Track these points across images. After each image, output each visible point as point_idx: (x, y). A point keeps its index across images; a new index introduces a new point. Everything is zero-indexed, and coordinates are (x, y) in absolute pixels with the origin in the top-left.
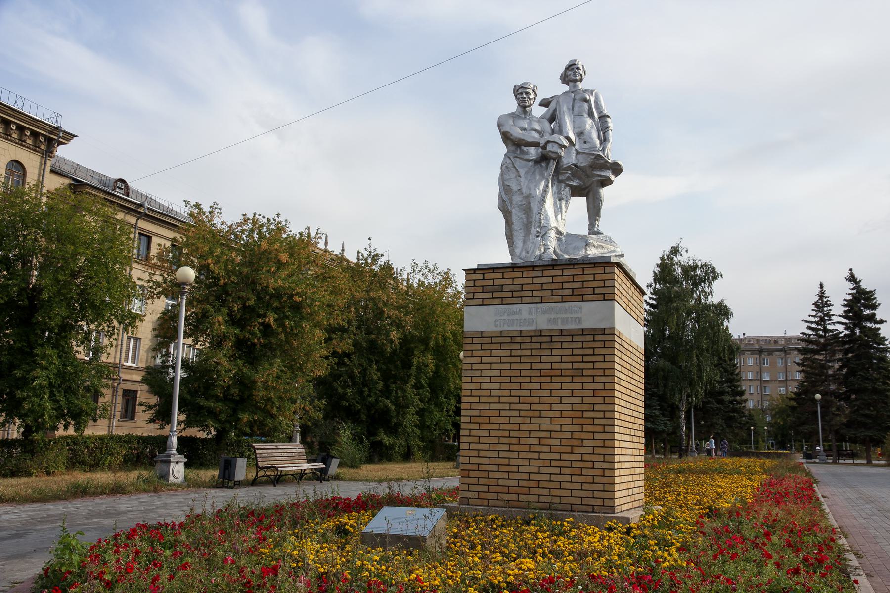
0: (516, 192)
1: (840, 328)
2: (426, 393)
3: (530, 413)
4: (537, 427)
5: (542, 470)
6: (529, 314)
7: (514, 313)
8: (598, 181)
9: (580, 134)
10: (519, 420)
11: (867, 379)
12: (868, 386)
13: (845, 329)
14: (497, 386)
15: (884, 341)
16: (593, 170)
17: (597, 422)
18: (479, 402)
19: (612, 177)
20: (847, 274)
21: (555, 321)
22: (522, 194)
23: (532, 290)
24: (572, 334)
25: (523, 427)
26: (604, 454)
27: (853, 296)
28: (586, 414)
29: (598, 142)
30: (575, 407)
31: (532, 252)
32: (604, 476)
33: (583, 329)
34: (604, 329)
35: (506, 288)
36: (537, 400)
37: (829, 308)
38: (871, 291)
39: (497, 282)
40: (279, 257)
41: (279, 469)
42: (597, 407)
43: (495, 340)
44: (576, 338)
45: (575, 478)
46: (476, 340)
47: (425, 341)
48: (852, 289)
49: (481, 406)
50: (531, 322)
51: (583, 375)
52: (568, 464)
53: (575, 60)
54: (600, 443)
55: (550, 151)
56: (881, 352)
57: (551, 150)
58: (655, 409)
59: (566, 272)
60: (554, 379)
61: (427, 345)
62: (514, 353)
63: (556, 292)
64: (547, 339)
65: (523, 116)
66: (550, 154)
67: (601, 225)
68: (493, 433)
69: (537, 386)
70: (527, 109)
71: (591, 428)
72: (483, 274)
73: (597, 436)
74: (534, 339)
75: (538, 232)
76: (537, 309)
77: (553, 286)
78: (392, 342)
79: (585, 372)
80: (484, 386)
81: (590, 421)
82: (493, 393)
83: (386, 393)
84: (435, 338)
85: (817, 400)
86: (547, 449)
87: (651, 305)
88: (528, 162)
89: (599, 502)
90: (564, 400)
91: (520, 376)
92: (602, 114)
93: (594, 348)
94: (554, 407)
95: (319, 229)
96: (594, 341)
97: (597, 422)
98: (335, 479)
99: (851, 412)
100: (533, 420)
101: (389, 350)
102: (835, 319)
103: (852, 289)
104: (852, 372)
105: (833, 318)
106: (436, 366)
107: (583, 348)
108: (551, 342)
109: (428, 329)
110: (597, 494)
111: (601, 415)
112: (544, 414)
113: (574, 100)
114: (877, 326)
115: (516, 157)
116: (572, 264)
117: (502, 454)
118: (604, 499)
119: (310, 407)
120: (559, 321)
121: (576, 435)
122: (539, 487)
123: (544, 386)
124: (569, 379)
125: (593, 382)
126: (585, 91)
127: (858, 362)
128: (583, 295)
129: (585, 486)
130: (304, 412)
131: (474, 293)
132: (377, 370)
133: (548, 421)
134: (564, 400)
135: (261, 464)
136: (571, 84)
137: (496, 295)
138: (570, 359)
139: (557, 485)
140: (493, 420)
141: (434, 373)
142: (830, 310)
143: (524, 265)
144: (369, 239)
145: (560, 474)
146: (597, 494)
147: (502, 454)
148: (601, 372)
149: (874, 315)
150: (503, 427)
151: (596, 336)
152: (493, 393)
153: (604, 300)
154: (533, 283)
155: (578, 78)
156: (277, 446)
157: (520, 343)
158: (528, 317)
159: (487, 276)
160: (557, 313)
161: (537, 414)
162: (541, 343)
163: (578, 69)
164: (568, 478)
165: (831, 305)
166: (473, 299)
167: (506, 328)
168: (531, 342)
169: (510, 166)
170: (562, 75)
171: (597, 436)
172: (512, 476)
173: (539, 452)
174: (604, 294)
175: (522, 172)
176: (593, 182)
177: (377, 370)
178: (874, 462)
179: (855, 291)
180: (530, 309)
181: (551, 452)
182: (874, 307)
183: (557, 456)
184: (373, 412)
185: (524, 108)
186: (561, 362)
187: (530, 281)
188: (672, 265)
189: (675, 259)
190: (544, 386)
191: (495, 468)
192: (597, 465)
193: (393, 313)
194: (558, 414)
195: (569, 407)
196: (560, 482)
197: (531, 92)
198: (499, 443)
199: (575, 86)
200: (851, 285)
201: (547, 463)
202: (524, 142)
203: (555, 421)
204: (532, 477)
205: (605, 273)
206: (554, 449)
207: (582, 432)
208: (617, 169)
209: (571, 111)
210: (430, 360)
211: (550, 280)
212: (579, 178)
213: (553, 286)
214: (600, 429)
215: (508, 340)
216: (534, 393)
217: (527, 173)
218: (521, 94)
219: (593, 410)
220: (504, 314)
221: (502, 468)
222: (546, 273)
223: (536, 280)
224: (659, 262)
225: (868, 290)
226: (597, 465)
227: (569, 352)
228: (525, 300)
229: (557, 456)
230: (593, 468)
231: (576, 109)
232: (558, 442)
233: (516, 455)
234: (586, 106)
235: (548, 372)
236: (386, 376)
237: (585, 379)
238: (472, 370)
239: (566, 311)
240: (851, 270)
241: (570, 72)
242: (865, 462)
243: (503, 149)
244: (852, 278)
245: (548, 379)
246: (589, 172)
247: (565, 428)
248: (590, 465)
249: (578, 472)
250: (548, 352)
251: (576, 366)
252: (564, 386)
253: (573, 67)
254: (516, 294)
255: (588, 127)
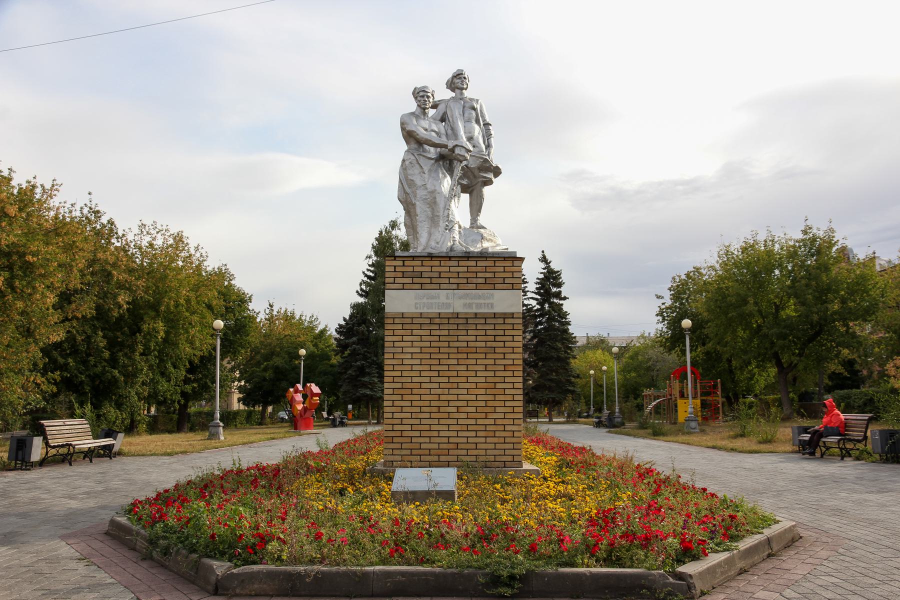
0: (420, 187)
1: (534, 303)
2: (154, 361)
3: (449, 386)
4: (455, 397)
5: (460, 434)
6: (447, 299)
7: (433, 298)
8: (483, 181)
9: (470, 139)
10: (439, 391)
11: (553, 348)
12: (554, 354)
13: (537, 304)
14: (418, 362)
15: (566, 315)
16: (480, 172)
17: (507, 392)
18: (402, 376)
19: (493, 179)
20: (540, 256)
21: (470, 305)
22: (427, 189)
23: (449, 278)
24: (485, 317)
25: (442, 398)
26: (514, 419)
27: (544, 276)
28: (498, 386)
29: (483, 147)
30: (489, 380)
31: (443, 243)
32: (514, 437)
33: (495, 313)
34: (513, 313)
35: (424, 275)
36: (455, 374)
37: (525, 285)
38: (558, 271)
39: (416, 269)
40: (6, 210)
41: (76, 447)
42: (507, 380)
43: (415, 321)
44: (489, 321)
45: (489, 440)
46: (397, 321)
47: (154, 307)
48: (544, 269)
49: (403, 380)
50: (448, 305)
51: (495, 353)
52: (483, 428)
53: (463, 70)
54: (510, 410)
55: (458, 154)
56: (564, 325)
57: (460, 153)
58: (374, 377)
59: (479, 263)
60: (470, 356)
61: (157, 311)
62: (433, 333)
63: (471, 281)
64: (464, 321)
65: (423, 117)
66: (459, 156)
67: (482, 220)
68: (414, 403)
69: (455, 362)
70: (426, 110)
71: (502, 398)
72: (404, 261)
73: (507, 404)
74: (452, 321)
75: (447, 226)
76: (454, 294)
77: (468, 275)
78: (120, 307)
79: (497, 350)
80: (405, 362)
81: (502, 392)
82: (414, 368)
83: (113, 362)
84: (168, 303)
85: (301, 356)
86: (464, 415)
87: (369, 277)
88: (430, 161)
89: (510, 458)
90: (479, 374)
91: (440, 353)
92: (485, 122)
93: (504, 330)
94: (470, 380)
95: (54, 180)
96: (504, 323)
97: (507, 392)
98: (118, 455)
99: (539, 377)
100: (451, 391)
101: (116, 314)
102: (529, 295)
103: (544, 269)
104: (541, 343)
105: (528, 293)
106: (167, 333)
107: (494, 329)
108: (467, 324)
109: (159, 295)
110: (507, 452)
111: (511, 386)
112: (461, 386)
113: (464, 107)
114: (561, 302)
115: (421, 155)
116: (468, 256)
117: (423, 421)
118: (513, 455)
119: (43, 379)
120: (474, 306)
121: (490, 404)
122: (457, 449)
123: (461, 362)
124: (483, 356)
125: (504, 359)
126: (471, 99)
127: (547, 334)
128: (494, 284)
129: (498, 446)
130: (34, 385)
131: (394, 278)
132: (104, 337)
133: (465, 391)
134: (479, 374)
135: (52, 443)
136: (458, 91)
137: (416, 280)
138: (484, 338)
139: (474, 446)
140: (415, 391)
141: (164, 339)
142: (526, 287)
143: (440, 255)
144: (90, 194)
145: (476, 437)
146: (507, 452)
147: (423, 421)
148: (510, 350)
149: (560, 292)
150: (423, 397)
151: (506, 320)
152: (414, 368)
153: (513, 289)
154: (449, 272)
155: (465, 86)
156: (64, 422)
157: (439, 324)
158: (445, 301)
159: (406, 263)
160: (472, 299)
161: (455, 385)
162: (458, 324)
163: (465, 78)
164: (483, 440)
165: (527, 282)
166: (394, 283)
167: (425, 310)
168: (448, 324)
169: (415, 162)
170: (448, 81)
171: (507, 404)
172: (433, 440)
173: (457, 419)
174: (513, 284)
175: (426, 169)
176: (478, 182)
177: (104, 337)
178: (554, 420)
179: (545, 271)
180: (447, 294)
181: (467, 418)
182: (559, 285)
183: (473, 422)
184: (97, 383)
185: (423, 110)
186: (476, 341)
187: (447, 269)
188: (390, 238)
189: (394, 232)
190: (461, 362)
191: (417, 434)
192: (508, 428)
193: (123, 277)
194: (474, 386)
195: (483, 380)
196: (476, 443)
197: (431, 96)
198: (421, 412)
199: (462, 94)
200: (543, 265)
201: (465, 428)
202: (431, 143)
203: (471, 391)
204: (451, 440)
205: (513, 266)
206: (470, 415)
207: (495, 400)
208: (497, 172)
209: (462, 117)
210: (160, 326)
211: (465, 269)
212: (468, 178)
213: (468, 275)
214: (510, 398)
215: (428, 321)
216: (451, 368)
217: (430, 171)
218: (423, 96)
219: (504, 382)
220: (423, 298)
221: (423, 434)
222: (461, 263)
223: (452, 269)
224: (377, 236)
225: (556, 270)
226: (508, 428)
227: (483, 333)
228: (442, 286)
229: (473, 422)
230: (504, 431)
231: (466, 115)
232: (474, 409)
233: (436, 422)
234: (474, 113)
235: (465, 350)
236: (112, 344)
237: (496, 356)
238: (394, 347)
239: (480, 297)
240: (543, 252)
241: (458, 81)
242: (547, 420)
243: (402, 147)
244: (544, 259)
245: (465, 356)
246: (476, 172)
247: (479, 398)
248: (502, 428)
249: (492, 434)
250: (464, 333)
251: (489, 344)
252: (479, 362)
253: (461, 76)
254: (434, 281)
255: (476, 134)
